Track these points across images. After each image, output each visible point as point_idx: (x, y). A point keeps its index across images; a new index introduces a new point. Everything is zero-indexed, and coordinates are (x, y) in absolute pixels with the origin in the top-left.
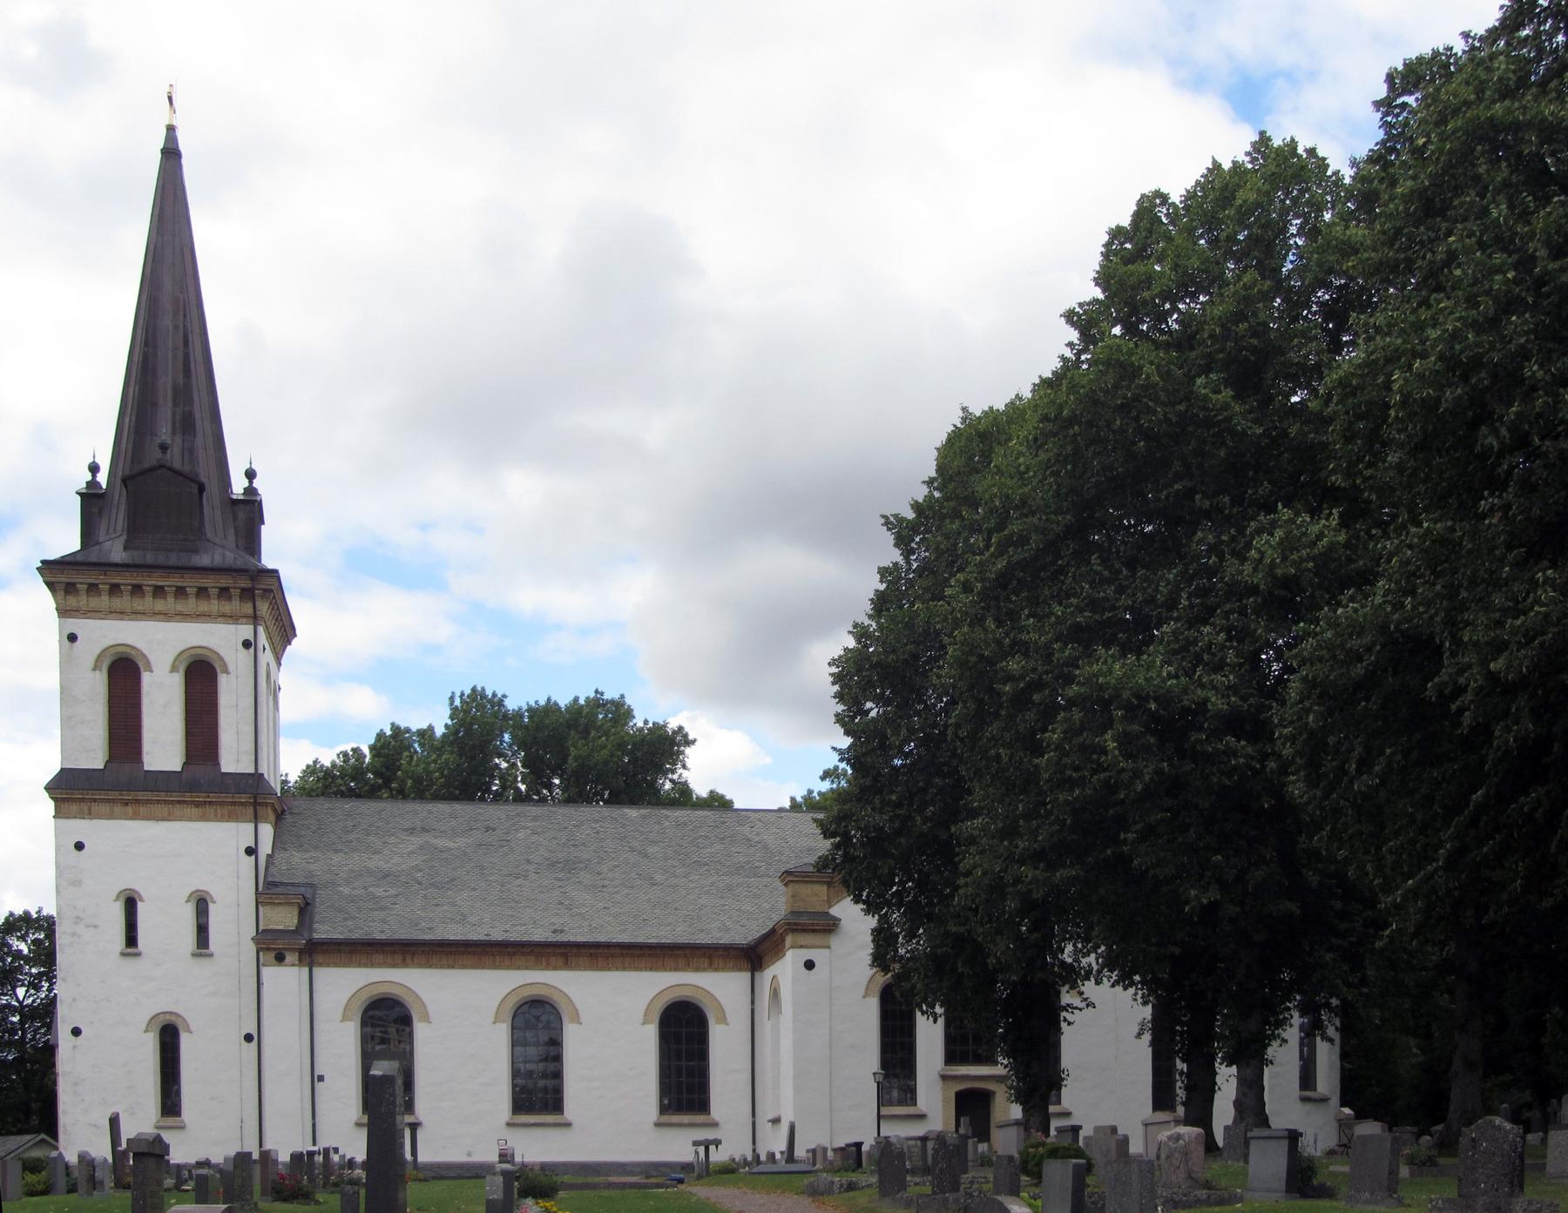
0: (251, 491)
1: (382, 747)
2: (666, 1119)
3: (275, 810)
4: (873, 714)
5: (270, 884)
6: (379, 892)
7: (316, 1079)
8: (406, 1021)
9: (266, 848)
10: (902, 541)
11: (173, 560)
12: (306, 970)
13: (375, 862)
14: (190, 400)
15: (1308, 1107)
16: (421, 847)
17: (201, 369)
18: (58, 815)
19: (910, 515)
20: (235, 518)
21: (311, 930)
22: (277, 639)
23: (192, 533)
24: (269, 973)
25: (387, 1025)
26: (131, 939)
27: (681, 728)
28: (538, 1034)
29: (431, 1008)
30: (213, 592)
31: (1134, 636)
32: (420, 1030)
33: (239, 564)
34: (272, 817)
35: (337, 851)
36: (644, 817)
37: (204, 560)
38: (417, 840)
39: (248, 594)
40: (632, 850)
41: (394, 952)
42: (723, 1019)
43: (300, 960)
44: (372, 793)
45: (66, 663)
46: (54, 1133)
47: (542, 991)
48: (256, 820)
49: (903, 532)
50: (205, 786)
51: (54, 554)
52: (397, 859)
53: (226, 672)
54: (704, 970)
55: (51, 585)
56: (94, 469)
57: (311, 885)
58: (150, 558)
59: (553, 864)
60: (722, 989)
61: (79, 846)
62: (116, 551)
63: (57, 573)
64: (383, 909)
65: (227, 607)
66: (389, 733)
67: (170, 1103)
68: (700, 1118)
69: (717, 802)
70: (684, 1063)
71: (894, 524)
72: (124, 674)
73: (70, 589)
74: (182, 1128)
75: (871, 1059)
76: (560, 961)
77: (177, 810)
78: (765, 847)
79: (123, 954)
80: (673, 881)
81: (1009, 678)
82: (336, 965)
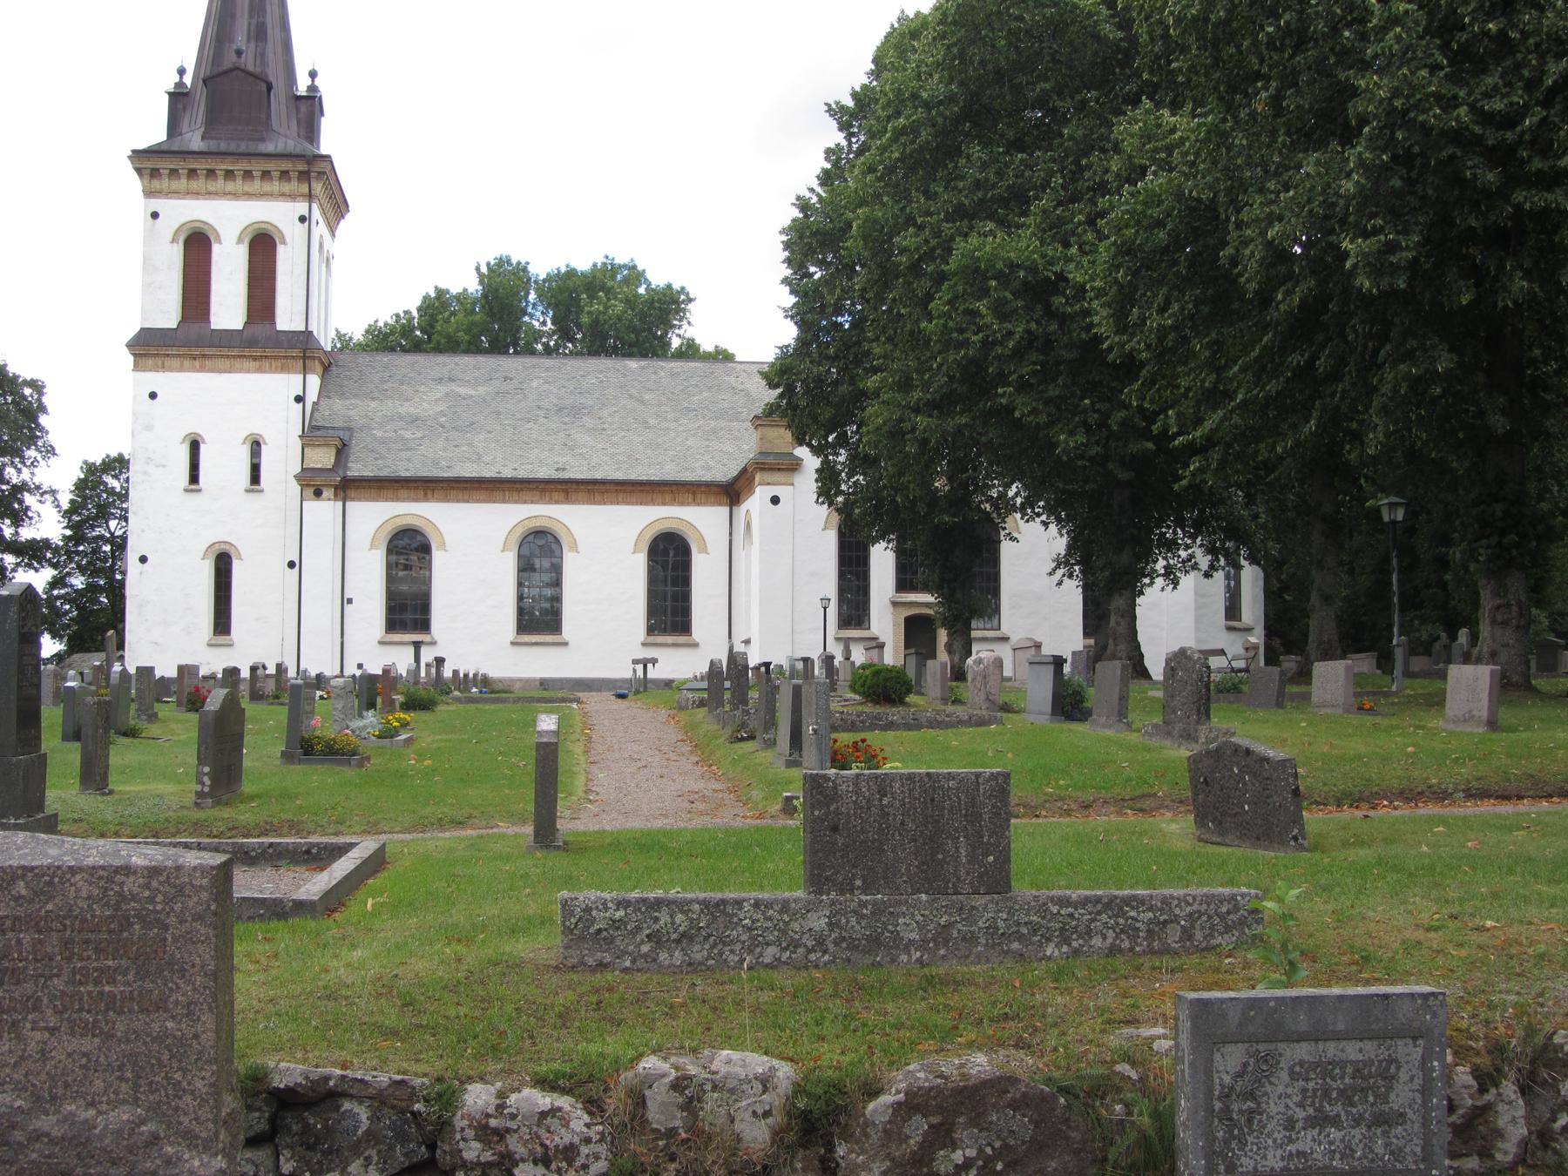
2: (652, 639)
3: (322, 363)
4: (816, 277)
5: (314, 428)
6: (408, 434)
7: (346, 601)
8: (425, 549)
10: (844, 127)
11: (243, 148)
12: (340, 504)
13: (406, 409)
16: (447, 395)
18: (137, 367)
19: (850, 103)
21: (346, 468)
22: (331, 214)
23: (262, 125)
24: (311, 506)
25: (409, 552)
26: (194, 478)
27: (683, 288)
28: (539, 557)
29: (447, 538)
31: (1009, 205)
32: (438, 557)
33: (298, 151)
34: (319, 369)
36: (643, 368)
37: (269, 147)
38: (442, 390)
39: (305, 176)
41: (416, 488)
42: (704, 549)
43: (336, 495)
44: (417, 347)
45: (149, 237)
49: (845, 118)
50: (264, 342)
51: (142, 145)
53: (284, 242)
54: (689, 504)
55: (138, 170)
56: (182, 72)
57: (350, 429)
58: (223, 147)
59: (560, 410)
60: (703, 522)
61: (153, 396)
62: (195, 142)
63: (149, 163)
64: (408, 449)
65: (287, 188)
67: (222, 622)
68: (682, 639)
69: (722, 356)
70: (669, 588)
71: (838, 112)
72: (197, 245)
75: (829, 585)
77: (238, 363)
78: (748, 395)
80: (664, 425)
81: (903, 251)
82: (367, 500)
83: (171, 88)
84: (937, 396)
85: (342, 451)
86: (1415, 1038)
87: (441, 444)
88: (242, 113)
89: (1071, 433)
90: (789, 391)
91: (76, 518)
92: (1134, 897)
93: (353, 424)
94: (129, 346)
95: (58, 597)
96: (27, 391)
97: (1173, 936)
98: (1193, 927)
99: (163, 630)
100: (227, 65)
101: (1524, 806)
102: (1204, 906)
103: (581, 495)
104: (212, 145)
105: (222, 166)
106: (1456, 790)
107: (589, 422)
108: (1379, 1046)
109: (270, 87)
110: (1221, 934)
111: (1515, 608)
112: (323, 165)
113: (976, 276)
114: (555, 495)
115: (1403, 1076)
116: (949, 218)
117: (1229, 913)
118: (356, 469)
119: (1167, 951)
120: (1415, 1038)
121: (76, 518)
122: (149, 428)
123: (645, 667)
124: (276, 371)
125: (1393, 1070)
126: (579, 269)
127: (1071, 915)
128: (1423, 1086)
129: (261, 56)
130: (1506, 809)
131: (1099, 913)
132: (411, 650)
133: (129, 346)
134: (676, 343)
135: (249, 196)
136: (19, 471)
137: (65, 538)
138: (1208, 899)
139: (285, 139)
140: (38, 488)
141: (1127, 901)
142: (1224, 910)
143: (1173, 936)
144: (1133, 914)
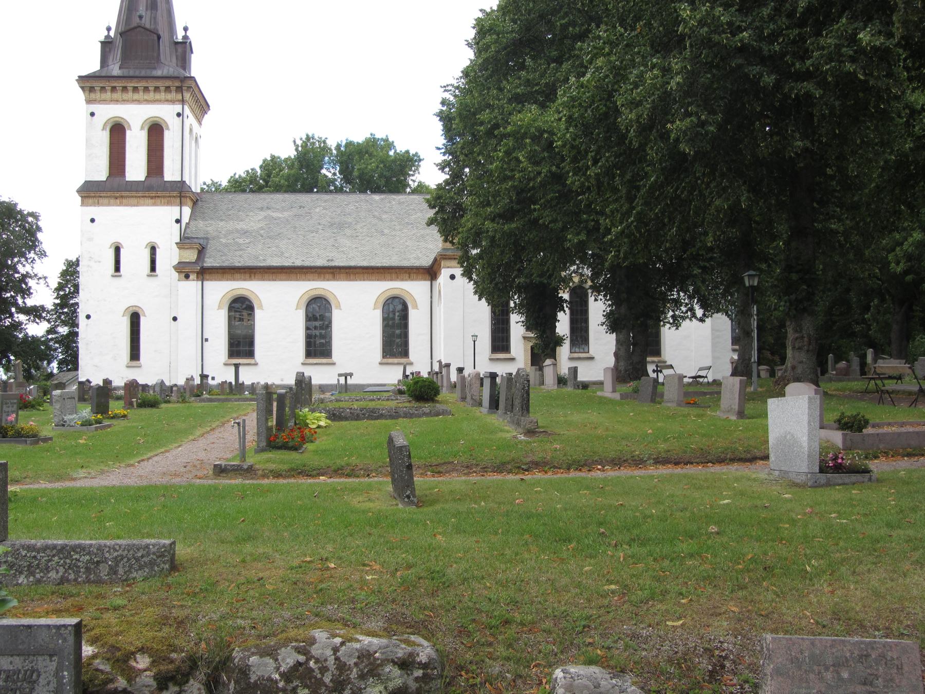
0: (186, 37)
2: (385, 360)
6: (241, 241)
7: (204, 340)
8: (250, 308)
9: (185, 220)
11: (143, 73)
12: (200, 283)
13: (241, 226)
16: (265, 217)
18: (83, 204)
20: (176, 51)
21: (204, 261)
22: (198, 111)
23: (156, 60)
25: (241, 309)
26: (117, 268)
27: (417, 153)
30: (162, 89)
32: (258, 312)
33: (176, 74)
34: (190, 203)
35: (222, 220)
37: (159, 73)
38: (263, 214)
39: (179, 89)
41: (245, 273)
42: (416, 307)
43: (197, 278)
44: (260, 189)
46: (76, 368)
48: (181, 205)
50: (158, 188)
54: (406, 280)
55: (82, 88)
57: (207, 239)
58: (131, 73)
59: (332, 225)
61: (93, 220)
62: (115, 70)
63: (89, 83)
66: (269, 159)
67: (135, 354)
72: (118, 131)
73: (92, 89)
74: (256, 364)
76: (331, 276)
77: (142, 201)
80: (393, 233)
82: (216, 280)
83: (102, 39)
84: (502, 211)
85: (201, 252)
86: (51, 656)
87: (260, 246)
88: (145, 54)
89: (578, 234)
90: (442, 210)
91: (62, 293)
92: (79, 546)
94: (78, 191)
95: (52, 339)
96: (30, 219)
97: (104, 571)
98: (117, 565)
99: (102, 359)
100: (134, 24)
101: (690, 470)
102: (126, 552)
104: (125, 72)
105: (131, 85)
106: (649, 459)
107: (348, 232)
108: (25, 660)
109: (159, 37)
110: (137, 571)
111: (806, 339)
112: (190, 82)
113: (519, 136)
114: (327, 276)
115: (42, 681)
116: (510, 101)
117: (142, 556)
118: (209, 262)
119: (99, 582)
120: (51, 656)
121: (62, 293)
123: (346, 378)
124: (162, 204)
125: (34, 677)
127: (35, 557)
128: (56, 688)
129: (154, 19)
130: (678, 470)
131: (54, 556)
132: (233, 368)
133: (78, 191)
134: (413, 185)
135: (148, 102)
136: (24, 266)
137: (55, 304)
138: (129, 548)
139: (169, 67)
140: (36, 275)
141: (74, 548)
142: (139, 554)
143: (104, 571)
144: (77, 556)
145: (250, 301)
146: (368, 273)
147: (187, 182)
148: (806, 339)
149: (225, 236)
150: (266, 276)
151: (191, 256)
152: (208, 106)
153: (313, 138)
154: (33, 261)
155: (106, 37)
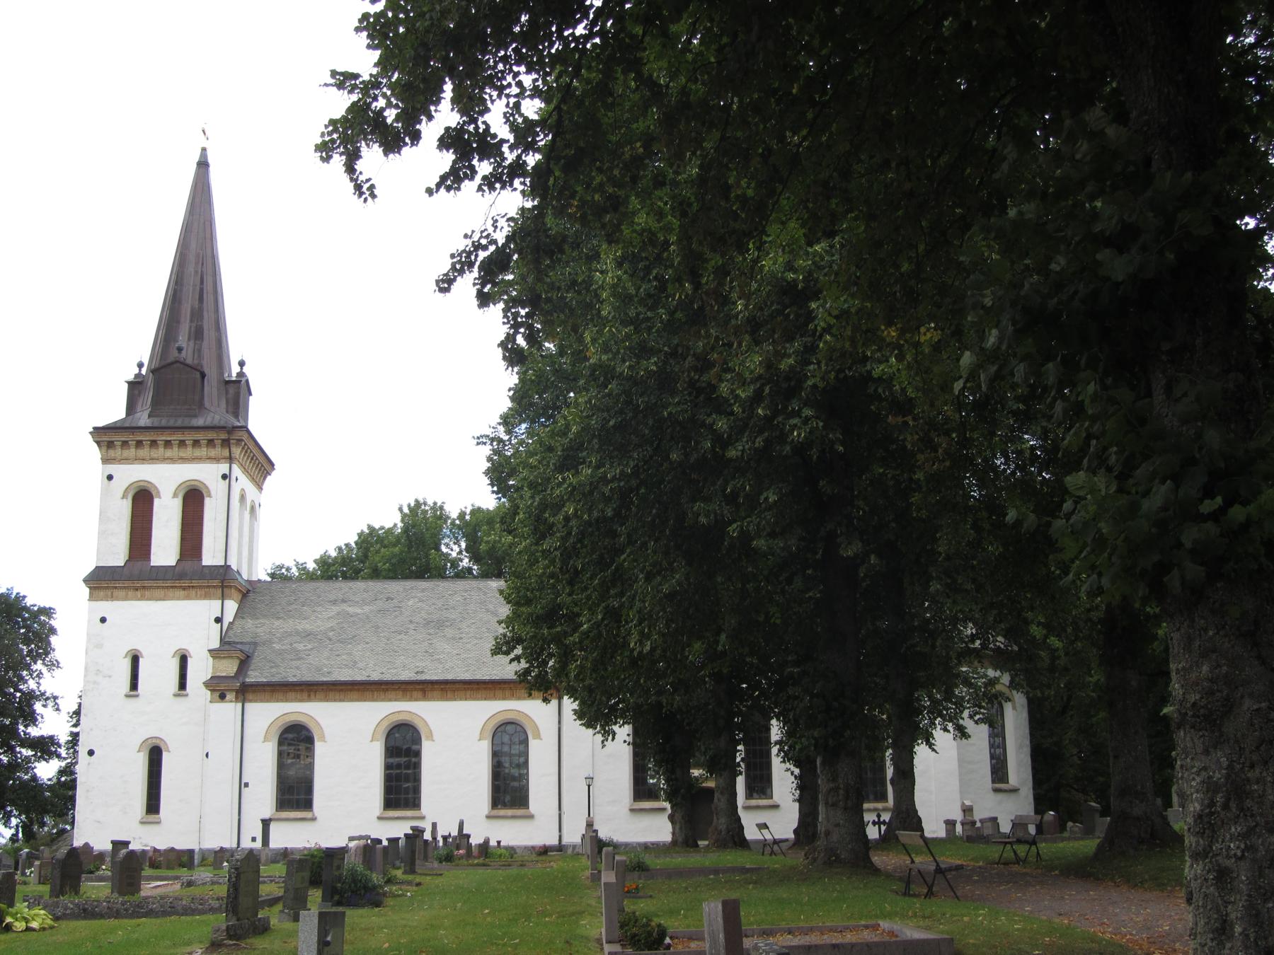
0: (241, 374)
1: (363, 542)
2: (496, 812)
6: (300, 647)
7: (243, 785)
9: (229, 618)
11: (179, 423)
12: (554, 702)
14: (201, 317)
15: (1000, 796)
16: (338, 614)
17: (211, 297)
18: (92, 598)
20: (227, 393)
21: (246, 675)
22: (255, 472)
23: (200, 406)
25: (296, 742)
26: (134, 685)
29: (327, 731)
32: (319, 747)
33: (222, 423)
35: (278, 618)
37: (200, 422)
38: (336, 609)
39: (226, 443)
40: (488, 610)
41: (302, 691)
43: (237, 698)
45: (105, 494)
47: (510, 716)
48: (223, 598)
50: (194, 575)
52: (319, 623)
53: (210, 496)
54: (524, 699)
55: (98, 443)
57: (255, 644)
58: (164, 423)
59: (428, 623)
61: (103, 620)
62: (143, 419)
63: (107, 437)
64: (299, 659)
66: (367, 531)
67: (153, 805)
72: (143, 499)
76: (420, 694)
77: (170, 593)
79: (127, 696)
83: (131, 377)
85: (244, 663)
87: (326, 654)
93: (258, 640)
94: (85, 581)
103: (436, 693)
104: (156, 422)
107: (449, 632)
109: (203, 376)
111: (841, 792)
112: (241, 433)
114: (415, 694)
118: (253, 676)
122: (99, 646)
124: (197, 598)
126: (484, 507)
129: (198, 352)
133: (85, 581)
139: (216, 414)
140: (43, 694)
145: (308, 730)
146: (472, 689)
147: (234, 567)
148: (841, 792)
149: (280, 640)
150: (331, 694)
151: (229, 667)
152: (272, 464)
153: (425, 504)
154: (40, 675)
155: (137, 376)
